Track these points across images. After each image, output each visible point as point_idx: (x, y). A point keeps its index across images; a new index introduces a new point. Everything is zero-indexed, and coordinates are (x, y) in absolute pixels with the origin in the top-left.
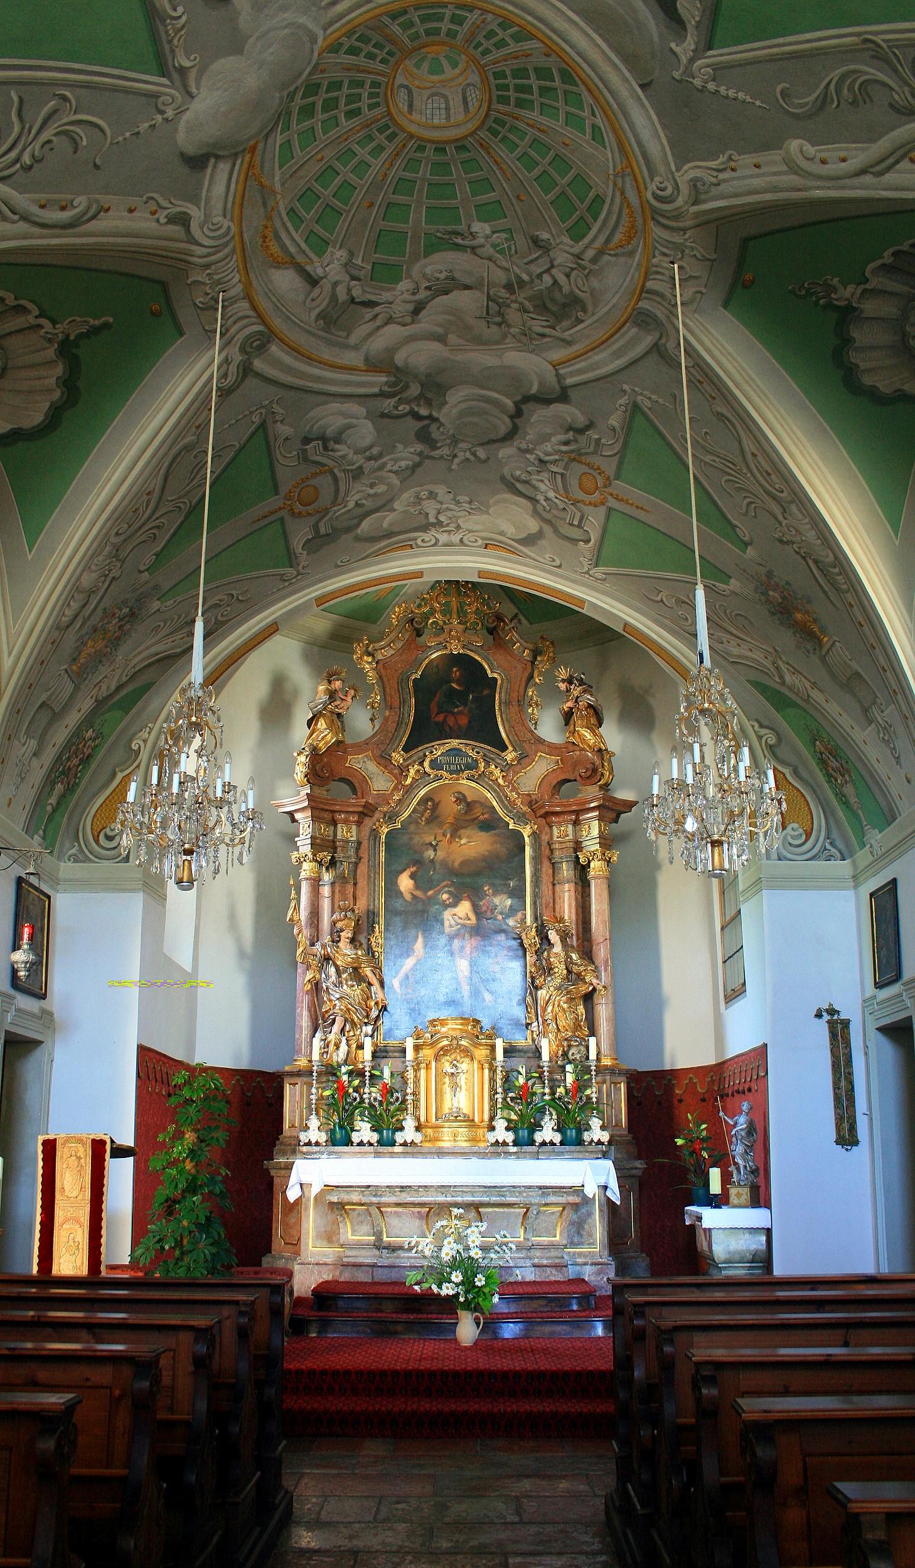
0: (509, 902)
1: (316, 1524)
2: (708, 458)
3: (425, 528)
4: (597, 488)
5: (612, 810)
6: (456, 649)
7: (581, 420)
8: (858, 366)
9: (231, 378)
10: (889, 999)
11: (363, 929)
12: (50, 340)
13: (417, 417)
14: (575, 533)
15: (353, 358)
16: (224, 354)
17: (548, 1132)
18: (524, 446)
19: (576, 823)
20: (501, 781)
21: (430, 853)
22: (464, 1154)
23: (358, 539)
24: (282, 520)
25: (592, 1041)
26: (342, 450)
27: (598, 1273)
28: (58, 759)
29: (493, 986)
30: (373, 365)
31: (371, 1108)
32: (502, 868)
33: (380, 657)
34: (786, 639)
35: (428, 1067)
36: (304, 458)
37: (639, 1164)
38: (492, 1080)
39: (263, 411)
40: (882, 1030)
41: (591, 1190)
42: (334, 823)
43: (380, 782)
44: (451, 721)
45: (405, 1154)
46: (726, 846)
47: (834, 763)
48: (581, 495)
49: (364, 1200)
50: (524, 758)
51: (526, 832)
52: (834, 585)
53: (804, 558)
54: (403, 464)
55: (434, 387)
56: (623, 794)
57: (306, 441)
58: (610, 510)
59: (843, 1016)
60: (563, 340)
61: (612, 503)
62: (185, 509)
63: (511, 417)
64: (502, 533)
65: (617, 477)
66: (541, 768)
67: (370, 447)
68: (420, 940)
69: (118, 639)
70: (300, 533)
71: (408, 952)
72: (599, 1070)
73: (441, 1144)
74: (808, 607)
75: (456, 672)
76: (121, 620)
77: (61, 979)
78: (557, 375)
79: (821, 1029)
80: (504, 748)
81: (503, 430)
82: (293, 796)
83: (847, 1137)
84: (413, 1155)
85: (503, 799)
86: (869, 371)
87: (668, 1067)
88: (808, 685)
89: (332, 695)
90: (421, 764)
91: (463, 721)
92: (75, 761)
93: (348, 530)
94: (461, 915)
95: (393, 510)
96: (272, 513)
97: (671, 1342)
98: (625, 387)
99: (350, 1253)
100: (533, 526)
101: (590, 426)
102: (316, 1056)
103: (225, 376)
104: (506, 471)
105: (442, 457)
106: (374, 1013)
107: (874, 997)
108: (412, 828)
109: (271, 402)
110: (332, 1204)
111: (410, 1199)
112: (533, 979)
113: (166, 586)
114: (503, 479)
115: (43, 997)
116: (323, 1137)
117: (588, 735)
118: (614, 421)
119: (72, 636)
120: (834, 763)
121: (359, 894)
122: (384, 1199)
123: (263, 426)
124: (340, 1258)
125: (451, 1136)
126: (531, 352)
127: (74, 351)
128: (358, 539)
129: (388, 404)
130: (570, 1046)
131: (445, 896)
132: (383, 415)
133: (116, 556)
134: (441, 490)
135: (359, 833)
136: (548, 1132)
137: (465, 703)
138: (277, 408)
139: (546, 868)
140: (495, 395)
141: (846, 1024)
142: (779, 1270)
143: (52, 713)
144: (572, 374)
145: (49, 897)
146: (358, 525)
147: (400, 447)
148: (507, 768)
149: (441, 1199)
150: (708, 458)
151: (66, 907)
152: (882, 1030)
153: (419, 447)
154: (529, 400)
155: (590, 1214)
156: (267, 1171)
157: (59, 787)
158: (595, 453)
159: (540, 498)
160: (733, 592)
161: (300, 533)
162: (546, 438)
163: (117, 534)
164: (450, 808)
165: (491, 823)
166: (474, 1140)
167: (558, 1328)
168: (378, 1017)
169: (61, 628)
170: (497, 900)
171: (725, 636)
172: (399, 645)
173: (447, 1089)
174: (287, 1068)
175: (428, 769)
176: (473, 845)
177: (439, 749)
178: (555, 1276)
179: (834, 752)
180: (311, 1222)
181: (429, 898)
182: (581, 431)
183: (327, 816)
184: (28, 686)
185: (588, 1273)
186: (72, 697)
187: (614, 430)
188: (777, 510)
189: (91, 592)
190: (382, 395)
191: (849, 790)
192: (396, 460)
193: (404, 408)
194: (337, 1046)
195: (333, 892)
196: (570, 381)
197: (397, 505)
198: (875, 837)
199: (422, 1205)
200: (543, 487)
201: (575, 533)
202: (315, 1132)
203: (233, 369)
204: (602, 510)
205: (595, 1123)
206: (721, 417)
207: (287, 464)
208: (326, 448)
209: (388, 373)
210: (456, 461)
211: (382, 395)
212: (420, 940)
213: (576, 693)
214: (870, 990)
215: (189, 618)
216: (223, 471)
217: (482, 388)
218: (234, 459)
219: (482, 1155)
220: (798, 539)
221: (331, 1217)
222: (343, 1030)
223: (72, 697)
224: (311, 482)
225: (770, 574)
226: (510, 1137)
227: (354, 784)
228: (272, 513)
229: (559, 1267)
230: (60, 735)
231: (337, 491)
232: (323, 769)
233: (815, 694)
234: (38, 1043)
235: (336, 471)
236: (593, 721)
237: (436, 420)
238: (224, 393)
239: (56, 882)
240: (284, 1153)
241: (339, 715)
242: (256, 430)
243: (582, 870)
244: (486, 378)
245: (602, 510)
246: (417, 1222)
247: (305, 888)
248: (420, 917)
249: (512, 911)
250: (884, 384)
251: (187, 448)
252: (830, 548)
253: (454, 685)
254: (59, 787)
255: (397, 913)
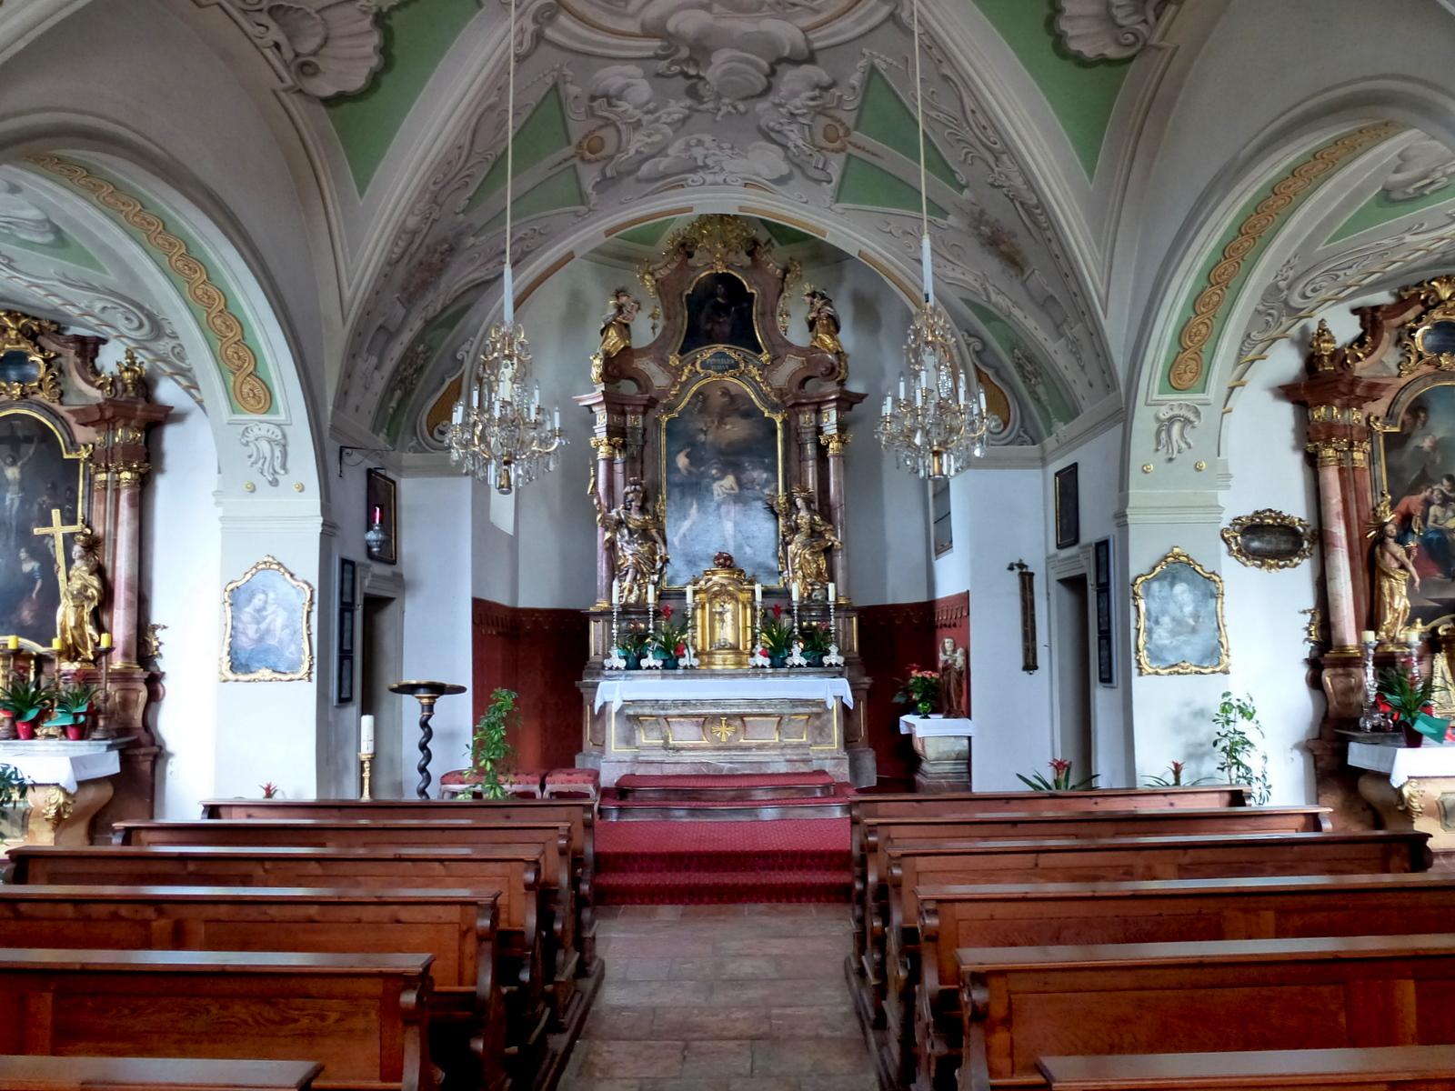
0: (765, 476)
1: (625, 982)
2: (933, 114)
3: (694, 170)
4: (838, 137)
5: (847, 401)
6: (721, 270)
7: (826, 79)
8: (1066, 33)
9: (526, 45)
10: (1070, 558)
11: (647, 500)
12: (364, 12)
13: (687, 76)
14: (819, 175)
15: (631, 26)
16: (519, 24)
17: (797, 658)
18: (777, 101)
19: (818, 412)
20: (758, 379)
21: (702, 437)
22: (733, 676)
23: (639, 180)
24: (574, 167)
25: (831, 586)
26: (623, 105)
27: (836, 765)
28: (396, 371)
29: (752, 542)
30: (647, 33)
31: (660, 635)
32: (759, 447)
33: (658, 276)
34: (993, 265)
35: (703, 607)
36: (591, 113)
37: (867, 680)
38: (754, 617)
39: (555, 74)
40: (1063, 581)
41: (832, 704)
42: (623, 414)
43: (660, 380)
44: (717, 328)
45: (685, 676)
46: (945, 456)
47: (1029, 368)
48: (825, 143)
49: (654, 712)
50: (776, 359)
51: (778, 420)
52: (1036, 223)
53: (1012, 200)
54: (676, 117)
55: (701, 50)
56: (855, 387)
57: (593, 98)
58: (849, 156)
59: (1030, 570)
60: (811, 9)
61: (851, 150)
62: (492, 159)
63: (767, 76)
64: (758, 175)
65: (856, 128)
66: (790, 366)
67: (647, 103)
68: (695, 506)
69: (441, 270)
70: (590, 176)
71: (685, 517)
72: (838, 607)
73: (714, 667)
74: (1014, 240)
75: (721, 288)
76: (442, 253)
77: (408, 544)
78: (807, 40)
79: (1014, 579)
80: (760, 351)
81: (760, 87)
82: (593, 396)
83: (1030, 665)
84: (693, 676)
85: (759, 392)
86: (1077, 37)
87: (890, 601)
88: (1010, 304)
89: (620, 308)
90: (693, 365)
91: (727, 329)
92: (411, 371)
93: (630, 173)
94: (727, 486)
95: (667, 156)
96: (566, 160)
97: (899, 866)
98: (865, 51)
99: (643, 753)
100: (784, 168)
101: (834, 84)
102: (615, 600)
103: (521, 44)
104: (763, 123)
105: (707, 111)
106: (659, 565)
107: (1056, 555)
108: (687, 417)
109: (562, 65)
110: (629, 717)
111: (690, 711)
112: (784, 536)
113: (478, 224)
114: (759, 129)
115: (393, 562)
116: (622, 664)
117: (827, 340)
118: (855, 79)
119: (401, 270)
120: (1029, 368)
121: (646, 472)
122: (670, 712)
123: (555, 87)
124: (636, 757)
125: (722, 661)
126: (785, 19)
127: (388, 22)
128: (639, 180)
129: (662, 66)
130: (813, 590)
131: (714, 472)
132: (658, 75)
133: (435, 202)
134: (707, 138)
135: (644, 421)
136: (797, 658)
137: (728, 313)
138: (567, 71)
139: (794, 448)
140: (753, 57)
141: (1032, 575)
142: (979, 786)
143: (388, 333)
144: (818, 39)
145: (394, 482)
146: (639, 168)
147: (673, 102)
148: (763, 367)
149: (714, 711)
150: (933, 114)
151: (409, 490)
152: (1063, 581)
153: (688, 102)
154: (780, 62)
155: (830, 721)
156: (578, 689)
157: (398, 393)
158: (838, 107)
159: (790, 144)
160: (951, 227)
161: (590, 176)
162: (795, 94)
163: (435, 183)
164: (717, 400)
165: (750, 413)
166: (739, 664)
167: (805, 812)
168: (662, 569)
169: (392, 263)
170: (755, 474)
171: (943, 262)
172: (674, 265)
173: (717, 625)
174: (592, 609)
175: (698, 368)
176: (735, 430)
177: (707, 353)
178: (803, 768)
179: (1030, 359)
180: (613, 729)
181: (702, 473)
182: (826, 88)
183: (618, 408)
184: (367, 313)
185: (828, 766)
186: (405, 318)
187: (854, 88)
188: (991, 160)
189: (415, 233)
190: (657, 57)
191: (1040, 390)
192: (669, 114)
193: (676, 68)
194: (631, 591)
195: (625, 469)
196: (817, 45)
197: (671, 151)
198: (1061, 428)
199: (699, 716)
200: (792, 136)
201: (819, 175)
202: (616, 660)
203: (527, 37)
204: (842, 156)
205: (833, 649)
206: (946, 78)
207: (579, 126)
208: (610, 104)
209: (661, 37)
210: (720, 113)
211: (657, 57)
212: (695, 506)
213: (818, 305)
214: (1053, 549)
215: (501, 249)
216: (523, 127)
217: (742, 50)
218: (531, 117)
219: (746, 675)
220: (1007, 184)
221: (629, 725)
222: (635, 579)
223: (405, 318)
224: (597, 134)
225: (982, 212)
226: (767, 662)
227: (642, 382)
228: (566, 160)
229: (805, 761)
230: (397, 351)
231: (620, 140)
232: (616, 369)
233: (1016, 311)
234: (390, 600)
235: (619, 124)
236: (832, 328)
237: (702, 78)
238: (520, 59)
239: (400, 470)
240: (591, 675)
241: (627, 326)
242: (549, 92)
243: (822, 451)
244: (743, 43)
245: (842, 156)
246: (695, 729)
247: (602, 467)
248: (694, 488)
249: (767, 483)
250: (1088, 50)
251: (491, 108)
252: (1034, 192)
253: (720, 300)
254: (398, 393)
255: (676, 485)
